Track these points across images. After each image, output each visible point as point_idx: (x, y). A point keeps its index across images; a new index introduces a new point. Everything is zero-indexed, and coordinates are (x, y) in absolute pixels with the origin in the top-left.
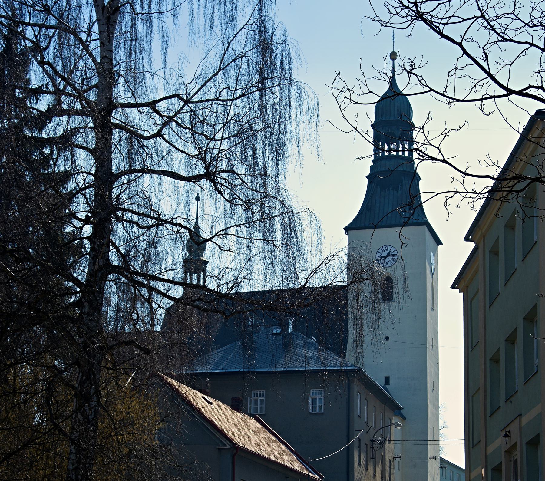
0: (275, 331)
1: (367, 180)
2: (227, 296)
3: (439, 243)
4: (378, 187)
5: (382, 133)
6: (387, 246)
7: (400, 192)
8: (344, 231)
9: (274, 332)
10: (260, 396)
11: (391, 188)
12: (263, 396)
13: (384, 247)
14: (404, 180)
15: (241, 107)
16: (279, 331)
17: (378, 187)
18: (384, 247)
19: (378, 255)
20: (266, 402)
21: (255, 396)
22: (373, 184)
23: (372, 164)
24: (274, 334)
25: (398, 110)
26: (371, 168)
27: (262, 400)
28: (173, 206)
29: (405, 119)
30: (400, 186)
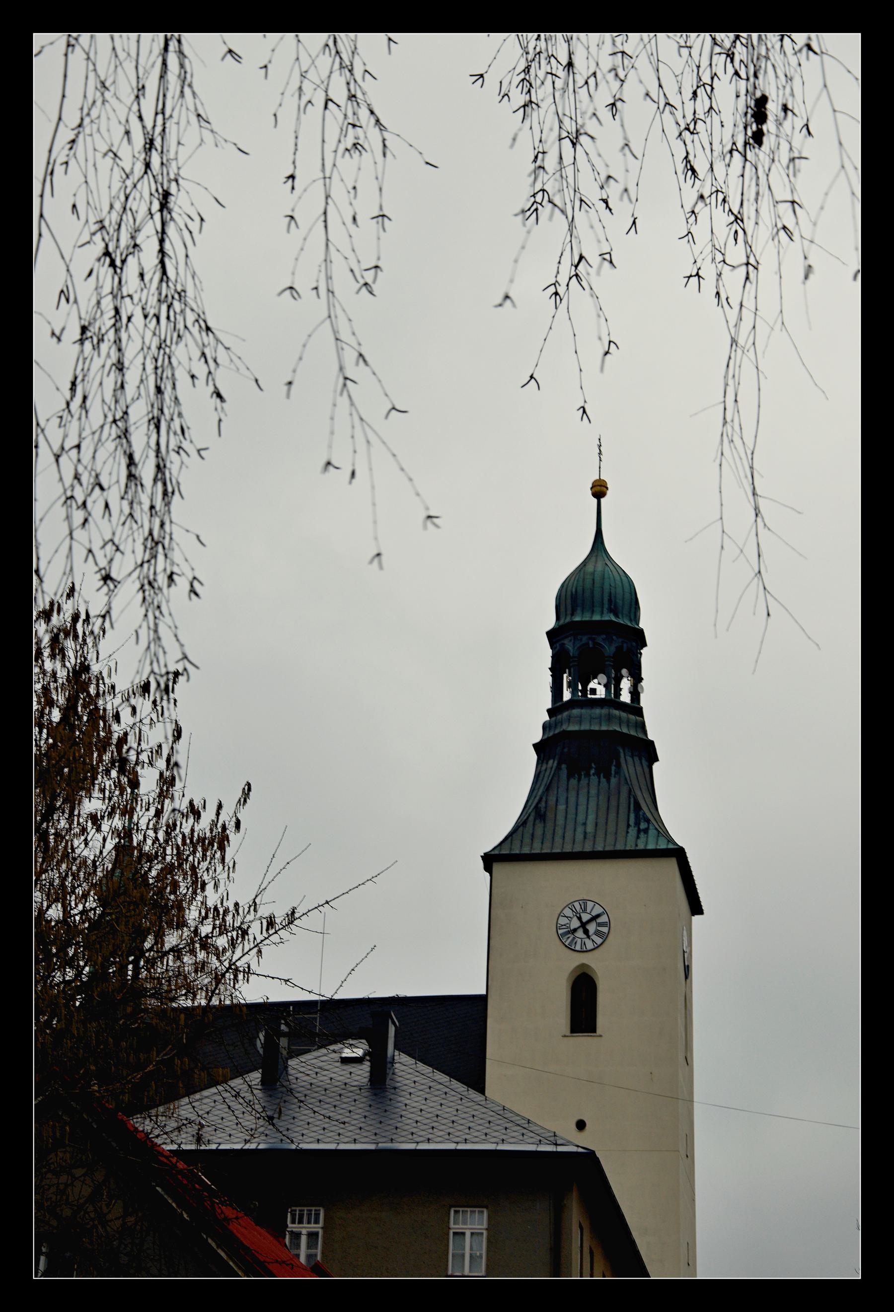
0: (347, 1053)
1: (534, 757)
2: (174, 1100)
3: (696, 908)
4: (564, 766)
5: (570, 646)
6: (585, 901)
7: (613, 781)
8: (481, 863)
9: (344, 1055)
10: (309, 1222)
11: (592, 771)
12: (316, 1222)
13: (577, 905)
14: (622, 755)
15: (347, 150)
16: (359, 1052)
17: (564, 766)
18: (577, 905)
19: (563, 921)
20: (324, 1243)
21: (293, 1222)
22: (551, 762)
23: (547, 718)
24: (346, 1061)
25: (610, 601)
26: (546, 727)
27: (312, 1236)
28: (104, 302)
29: (624, 621)
30: (613, 768)
